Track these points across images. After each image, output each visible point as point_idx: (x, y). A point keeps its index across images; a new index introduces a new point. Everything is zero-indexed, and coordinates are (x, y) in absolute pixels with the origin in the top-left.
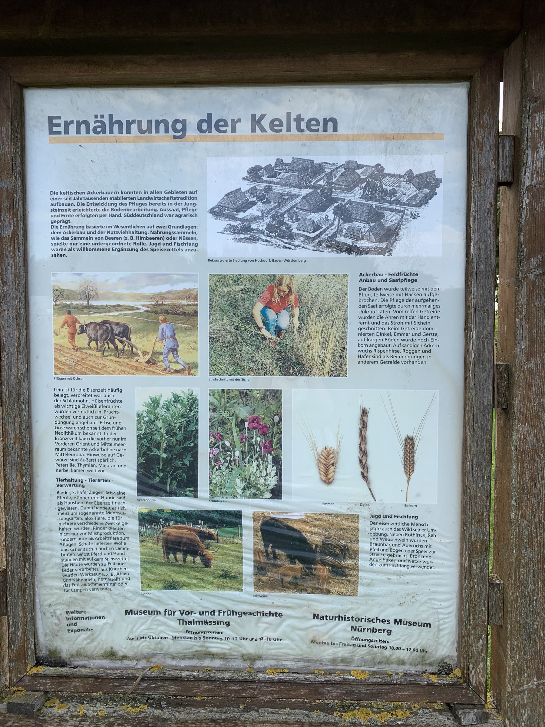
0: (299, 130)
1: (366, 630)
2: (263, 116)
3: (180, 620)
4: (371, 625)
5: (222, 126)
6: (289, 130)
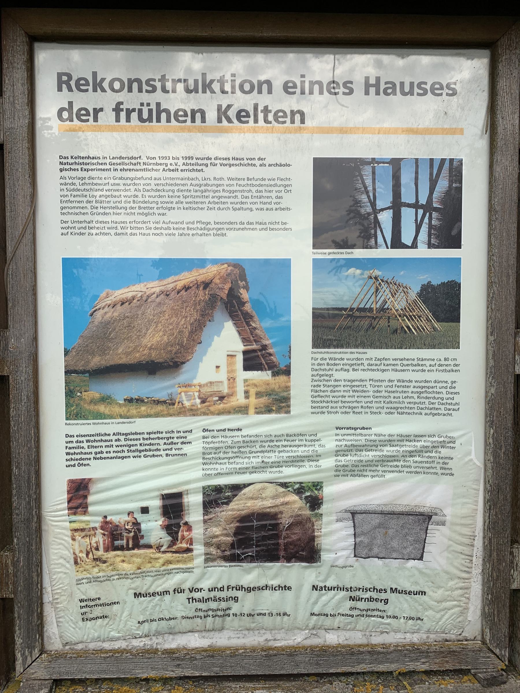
0: (266, 121)
1: (363, 600)
2: (229, 107)
3: (189, 599)
4: (368, 595)
5: (244, 117)
6: (256, 121)
